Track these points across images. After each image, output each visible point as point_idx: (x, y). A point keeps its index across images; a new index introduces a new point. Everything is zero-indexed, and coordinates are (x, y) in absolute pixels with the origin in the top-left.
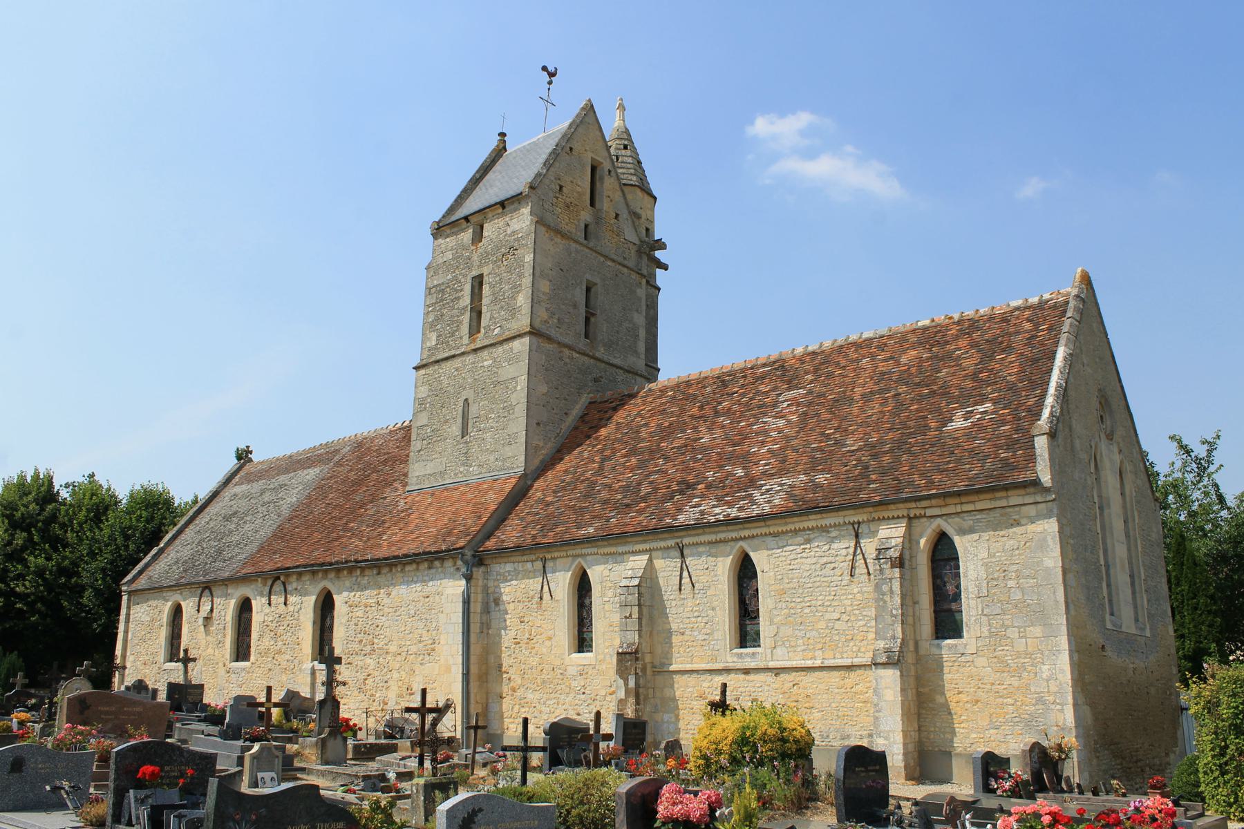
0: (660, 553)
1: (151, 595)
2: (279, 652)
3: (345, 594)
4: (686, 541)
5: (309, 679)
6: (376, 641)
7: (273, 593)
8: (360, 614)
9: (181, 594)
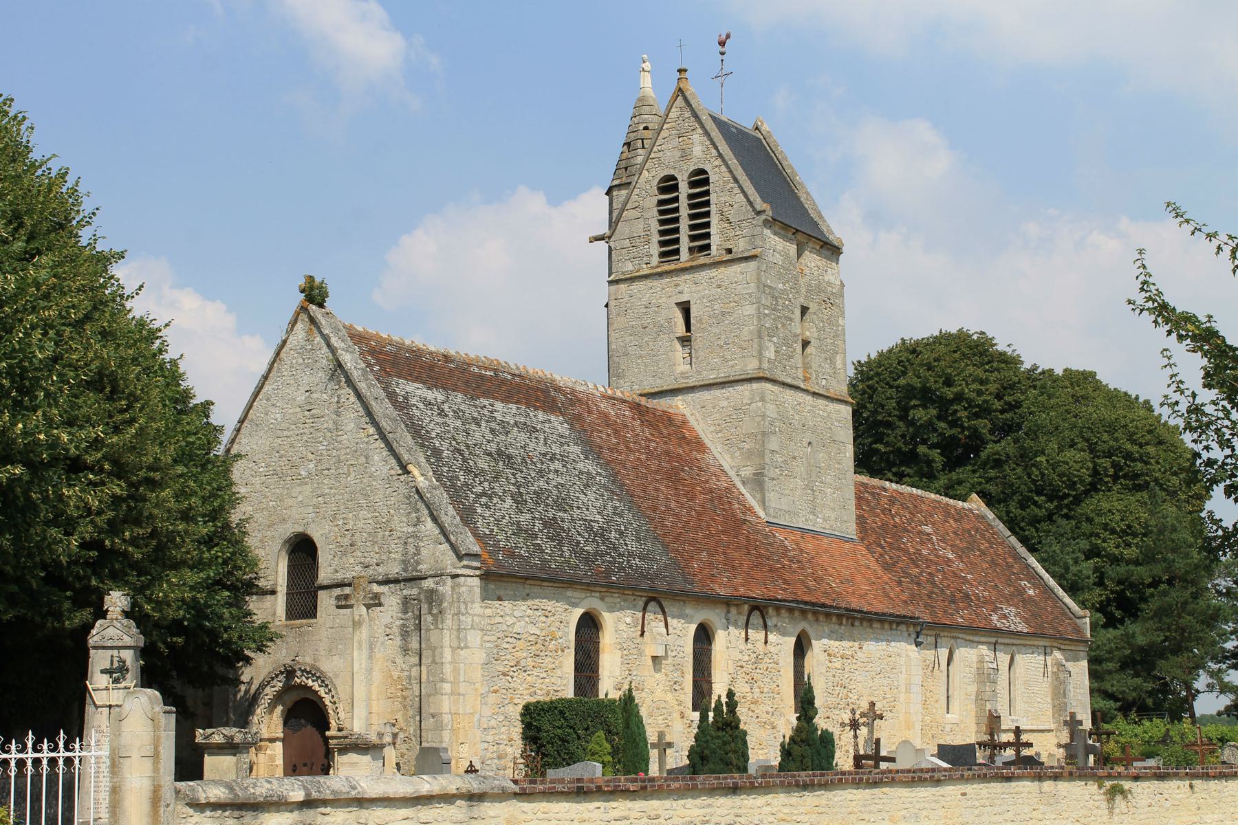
0: (1002, 647)
1: (537, 590)
2: (755, 702)
3: (825, 641)
4: (1000, 640)
5: (622, 286)
6: (850, 695)
7: (750, 626)
8: (838, 665)
9: (602, 599)
